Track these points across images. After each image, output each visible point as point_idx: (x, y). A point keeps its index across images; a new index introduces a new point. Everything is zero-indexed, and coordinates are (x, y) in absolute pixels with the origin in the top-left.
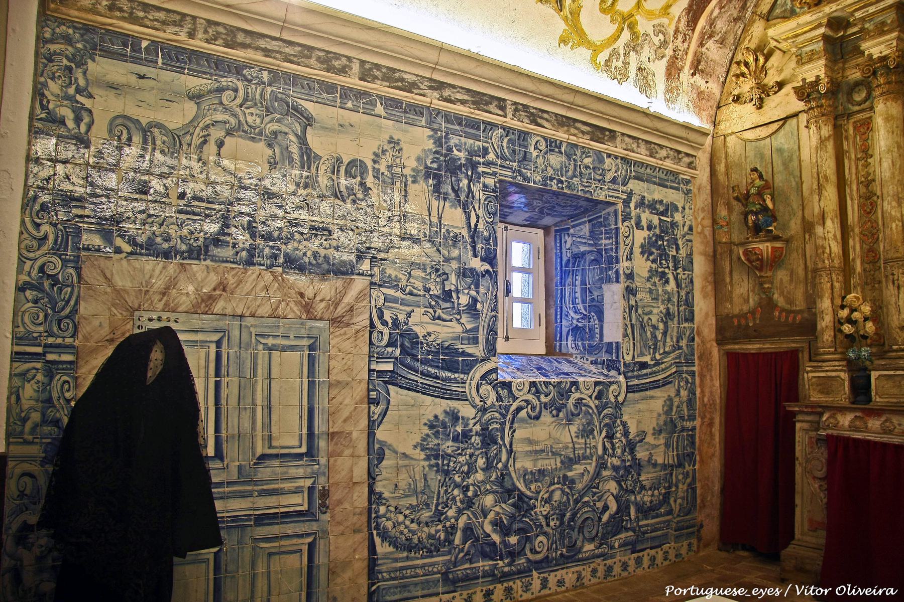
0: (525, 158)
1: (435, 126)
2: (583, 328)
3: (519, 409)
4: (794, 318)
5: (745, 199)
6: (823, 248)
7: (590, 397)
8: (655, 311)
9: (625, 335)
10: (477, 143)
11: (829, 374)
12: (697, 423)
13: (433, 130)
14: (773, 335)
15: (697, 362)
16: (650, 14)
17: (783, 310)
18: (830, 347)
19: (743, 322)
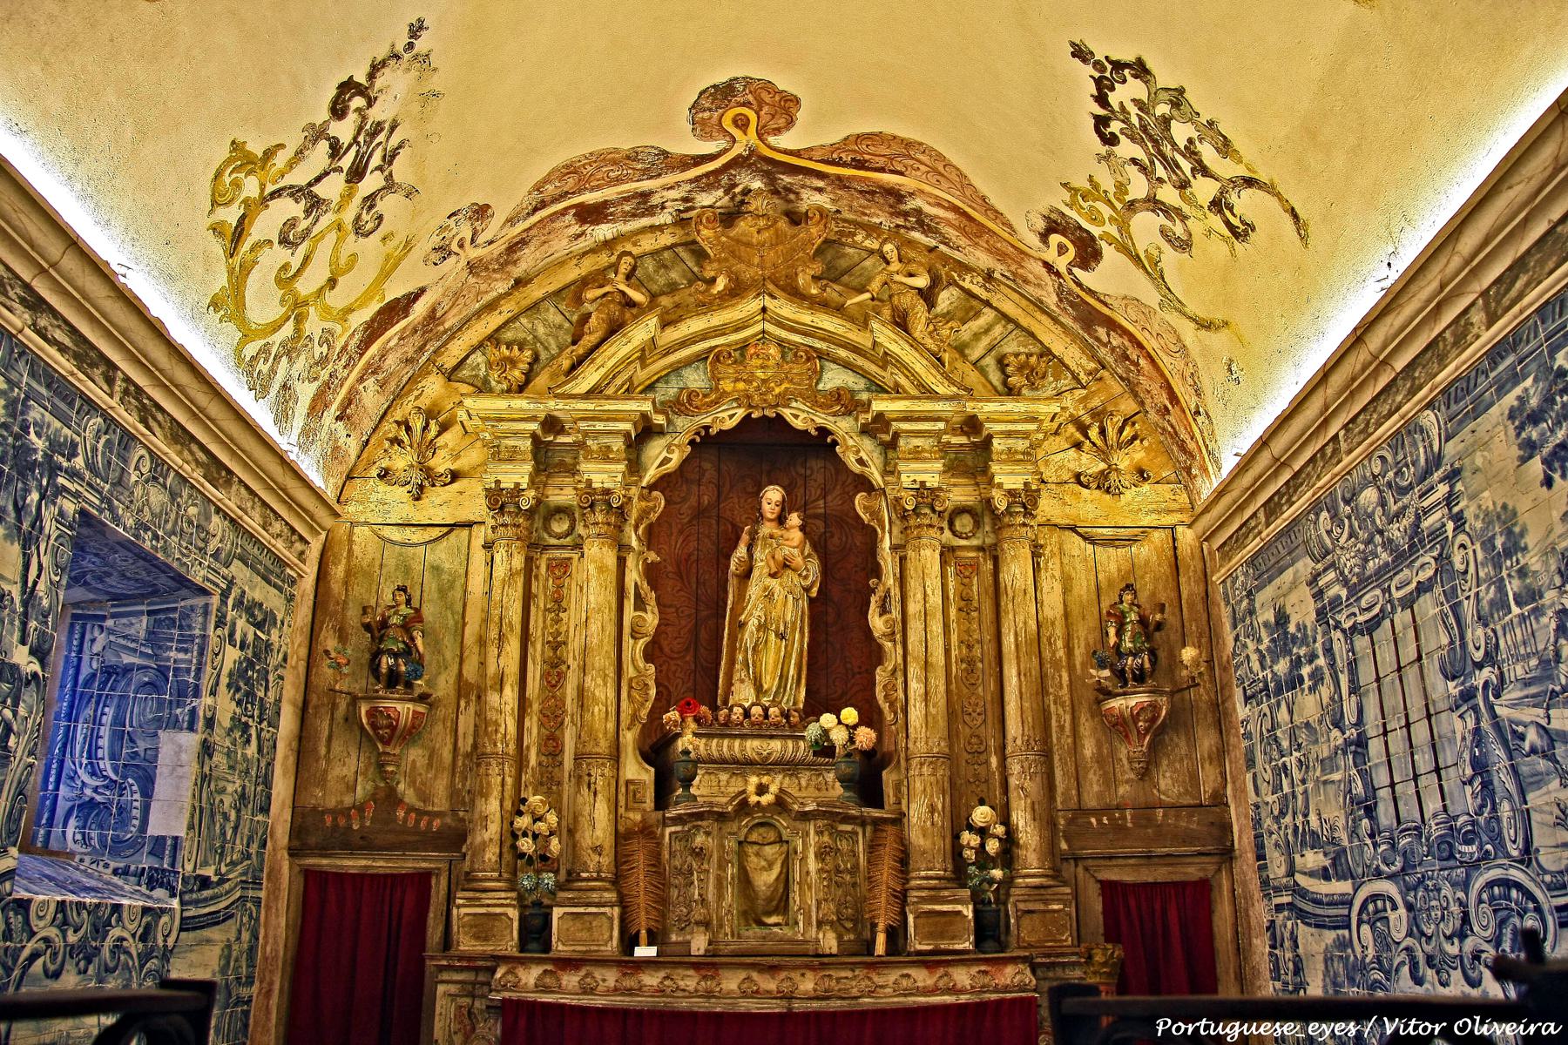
0: (119, 483)
1: (14, 376)
2: (106, 806)
3: (34, 956)
4: (430, 823)
5: (377, 630)
6: (497, 724)
7: (134, 935)
8: (230, 788)
9: (191, 827)
10: (66, 431)
11: (492, 910)
12: (255, 989)
13: (8, 381)
14: (391, 847)
15: (264, 882)
16: (327, 312)
17: (411, 809)
18: (493, 870)
19: (342, 822)
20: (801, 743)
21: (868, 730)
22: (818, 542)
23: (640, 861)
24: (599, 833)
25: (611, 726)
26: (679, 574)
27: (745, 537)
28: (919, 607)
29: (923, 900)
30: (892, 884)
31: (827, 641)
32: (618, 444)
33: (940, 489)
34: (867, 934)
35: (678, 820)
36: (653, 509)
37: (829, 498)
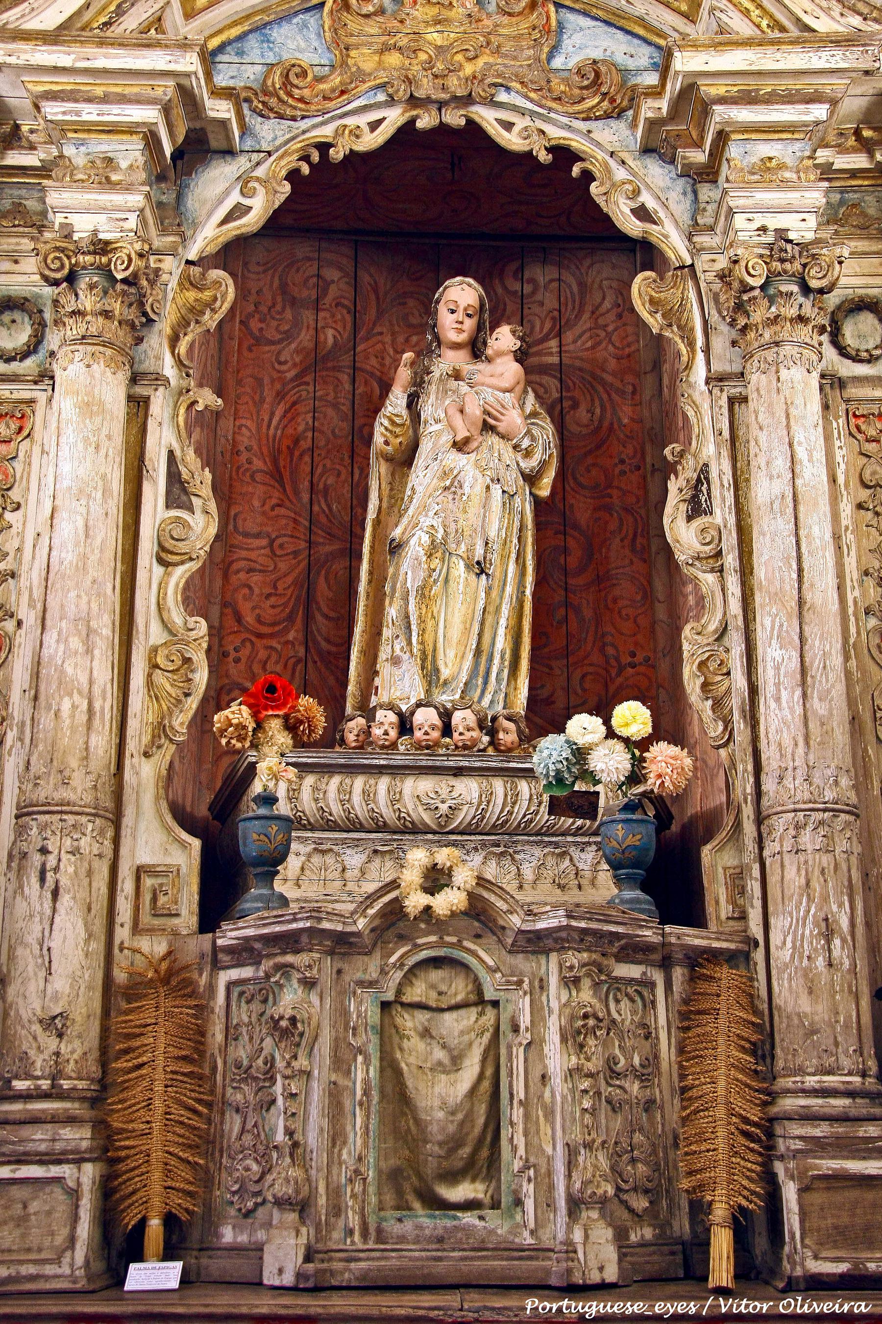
20: (524, 787)
21: (674, 750)
22: (555, 385)
23: (159, 1047)
24: (60, 984)
25: (102, 742)
26: (276, 475)
27: (404, 374)
28: (781, 486)
29: (818, 1146)
30: (740, 1105)
31: (567, 605)
32: (130, 154)
33: (817, 242)
34: (682, 1226)
35: (244, 952)
36: (210, 305)
37: (569, 336)
